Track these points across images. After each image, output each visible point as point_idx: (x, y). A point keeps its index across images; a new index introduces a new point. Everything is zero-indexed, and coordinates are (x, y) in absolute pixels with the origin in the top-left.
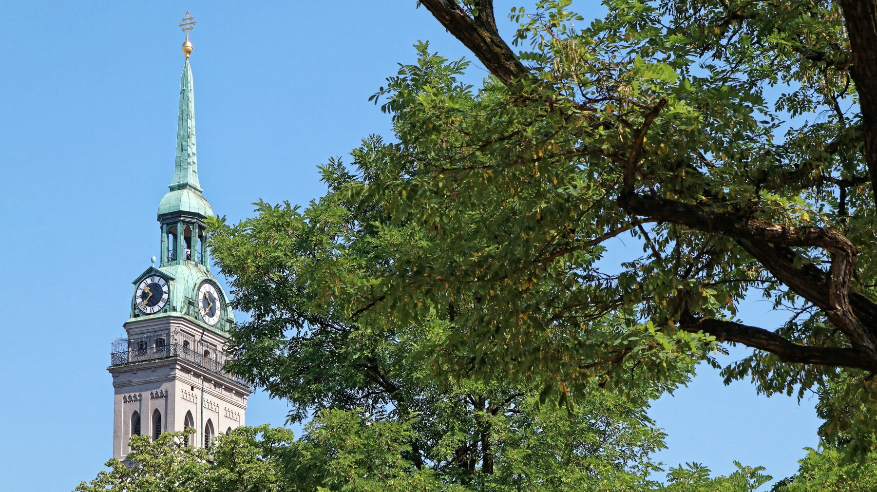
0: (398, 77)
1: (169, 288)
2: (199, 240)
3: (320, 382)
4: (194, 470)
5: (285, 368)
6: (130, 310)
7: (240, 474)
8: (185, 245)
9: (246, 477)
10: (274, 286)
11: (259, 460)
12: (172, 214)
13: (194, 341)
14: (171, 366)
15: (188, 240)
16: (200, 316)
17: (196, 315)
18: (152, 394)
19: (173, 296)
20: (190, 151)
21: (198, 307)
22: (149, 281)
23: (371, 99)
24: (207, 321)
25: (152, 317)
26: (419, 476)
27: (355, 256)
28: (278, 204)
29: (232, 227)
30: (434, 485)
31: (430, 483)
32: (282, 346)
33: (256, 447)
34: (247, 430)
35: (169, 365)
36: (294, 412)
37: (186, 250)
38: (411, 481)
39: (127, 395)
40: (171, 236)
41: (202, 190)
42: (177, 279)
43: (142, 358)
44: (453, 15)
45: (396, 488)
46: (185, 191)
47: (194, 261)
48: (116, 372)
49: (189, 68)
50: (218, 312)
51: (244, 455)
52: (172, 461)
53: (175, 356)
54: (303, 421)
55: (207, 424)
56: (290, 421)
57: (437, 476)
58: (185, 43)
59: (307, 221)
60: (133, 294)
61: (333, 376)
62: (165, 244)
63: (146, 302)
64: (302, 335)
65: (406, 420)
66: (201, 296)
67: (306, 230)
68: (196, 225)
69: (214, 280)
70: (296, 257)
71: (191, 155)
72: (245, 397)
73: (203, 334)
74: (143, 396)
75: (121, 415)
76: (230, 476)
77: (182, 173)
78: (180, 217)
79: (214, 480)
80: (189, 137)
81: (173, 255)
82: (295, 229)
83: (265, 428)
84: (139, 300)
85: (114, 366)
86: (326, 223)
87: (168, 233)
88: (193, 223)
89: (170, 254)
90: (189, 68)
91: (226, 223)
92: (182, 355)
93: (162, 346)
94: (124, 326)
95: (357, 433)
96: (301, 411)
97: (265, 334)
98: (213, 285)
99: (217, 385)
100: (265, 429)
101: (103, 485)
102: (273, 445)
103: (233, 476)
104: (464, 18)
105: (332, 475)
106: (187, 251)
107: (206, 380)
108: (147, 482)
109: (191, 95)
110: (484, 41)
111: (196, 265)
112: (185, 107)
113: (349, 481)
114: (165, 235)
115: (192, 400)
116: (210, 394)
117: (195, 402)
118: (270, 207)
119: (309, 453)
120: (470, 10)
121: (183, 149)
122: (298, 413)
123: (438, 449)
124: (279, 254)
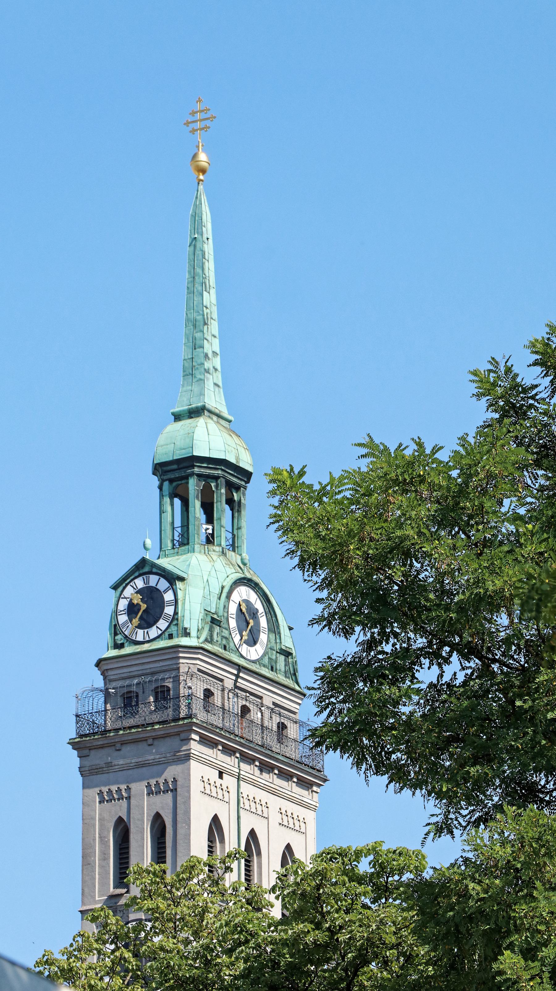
2: (227, 508)
6: (107, 636)
7: (332, 932)
8: (203, 518)
11: (365, 906)
13: (223, 690)
14: (183, 736)
16: (232, 645)
17: (224, 642)
18: (149, 786)
21: (228, 629)
22: (140, 583)
24: (244, 654)
25: (146, 647)
27: (545, 535)
28: (400, 445)
29: (317, 487)
33: (360, 884)
34: (342, 853)
35: (178, 734)
36: (440, 819)
37: (205, 526)
39: (105, 789)
40: (177, 501)
41: (230, 418)
43: (131, 722)
46: (201, 421)
47: (220, 545)
48: (85, 748)
49: (204, 199)
50: (263, 637)
51: (337, 898)
52: (205, 910)
53: (190, 716)
55: (248, 839)
56: (432, 834)
58: (195, 156)
59: (455, 473)
60: (113, 606)
63: (136, 621)
64: (447, 678)
66: (233, 609)
68: (222, 481)
69: (255, 579)
71: (210, 355)
72: (315, 788)
73: (237, 676)
74: (133, 792)
75: (94, 825)
77: (196, 388)
78: (193, 466)
79: (284, 943)
80: (205, 324)
81: (182, 535)
82: (432, 487)
83: (374, 849)
84: (123, 619)
85: (81, 736)
87: (173, 495)
88: (216, 478)
89: (176, 534)
90: (204, 199)
91: (306, 479)
92: (201, 716)
93: (165, 699)
94: (98, 665)
96: (452, 816)
98: (253, 588)
99: (265, 768)
100: (374, 850)
101: (84, 956)
102: (390, 879)
103: (321, 937)
107: (246, 759)
109: (209, 248)
111: (223, 553)
112: (199, 270)
114: (167, 500)
116: (254, 784)
117: (226, 799)
118: (386, 449)
121: (196, 345)
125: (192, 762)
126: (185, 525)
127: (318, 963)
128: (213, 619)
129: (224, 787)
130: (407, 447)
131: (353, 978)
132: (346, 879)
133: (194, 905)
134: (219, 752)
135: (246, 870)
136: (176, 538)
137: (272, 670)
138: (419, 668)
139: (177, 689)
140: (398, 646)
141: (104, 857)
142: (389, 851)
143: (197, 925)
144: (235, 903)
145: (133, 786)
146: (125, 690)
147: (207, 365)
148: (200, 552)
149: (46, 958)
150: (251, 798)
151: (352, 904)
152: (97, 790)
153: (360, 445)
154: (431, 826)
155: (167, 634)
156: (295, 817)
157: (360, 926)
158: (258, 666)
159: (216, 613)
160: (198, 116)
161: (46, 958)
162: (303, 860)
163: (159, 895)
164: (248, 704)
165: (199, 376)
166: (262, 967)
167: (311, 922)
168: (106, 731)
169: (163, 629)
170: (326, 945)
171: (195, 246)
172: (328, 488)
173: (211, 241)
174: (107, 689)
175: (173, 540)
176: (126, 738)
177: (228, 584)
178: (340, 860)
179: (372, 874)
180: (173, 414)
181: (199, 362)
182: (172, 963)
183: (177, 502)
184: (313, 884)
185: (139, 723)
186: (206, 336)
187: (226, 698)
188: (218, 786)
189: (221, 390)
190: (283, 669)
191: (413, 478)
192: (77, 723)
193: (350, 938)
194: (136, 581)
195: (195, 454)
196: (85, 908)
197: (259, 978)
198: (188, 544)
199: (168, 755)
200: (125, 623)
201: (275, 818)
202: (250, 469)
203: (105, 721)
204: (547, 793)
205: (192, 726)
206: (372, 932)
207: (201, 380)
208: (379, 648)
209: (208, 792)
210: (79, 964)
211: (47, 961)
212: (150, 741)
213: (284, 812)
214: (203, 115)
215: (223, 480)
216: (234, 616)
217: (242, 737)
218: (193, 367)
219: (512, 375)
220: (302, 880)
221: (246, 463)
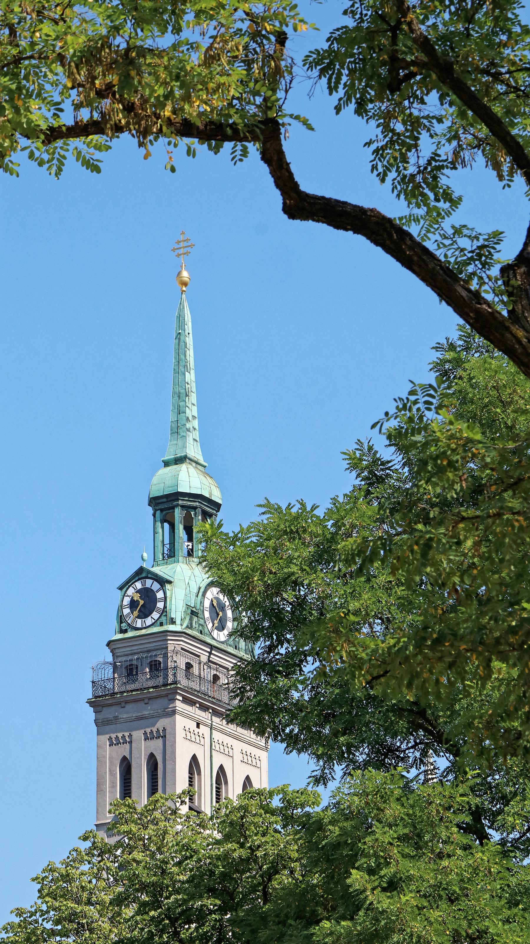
0: (407, 399)
1: (165, 593)
3: (351, 733)
4: (193, 846)
5: (305, 715)
6: (115, 624)
8: (185, 537)
9: (260, 853)
10: (289, 609)
11: (276, 831)
12: (167, 496)
13: (200, 663)
14: (170, 697)
15: (189, 530)
16: (206, 630)
17: (201, 628)
18: (145, 733)
19: (171, 604)
20: (189, 414)
21: (204, 618)
22: (139, 585)
23: (373, 427)
25: (143, 632)
26: (480, 854)
28: (290, 504)
29: (231, 535)
30: (502, 866)
31: (496, 863)
32: (300, 687)
35: (167, 695)
36: (318, 773)
37: (186, 544)
38: (471, 862)
39: (113, 736)
40: (166, 525)
42: (176, 582)
43: (132, 687)
44: (479, 313)
45: (451, 870)
46: (184, 467)
48: (99, 706)
49: (186, 304)
51: (256, 825)
52: (165, 832)
53: (175, 683)
54: (330, 784)
56: (312, 784)
57: (505, 854)
58: (179, 273)
60: (119, 602)
61: (367, 725)
62: (159, 536)
63: (136, 613)
65: (462, 782)
66: (207, 604)
67: (329, 536)
68: (199, 511)
70: (315, 572)
71: (190, 418)
73: (210, 653)
74: (134, 737)
75: (106, 762)
76: (239, 853)
77: (180, 442)
78: (178, 500)
79: (218, 858)
80: (187, 395)
83: (283, 790)
84: (126, 611)
85: (96, 697)
86: (353, 526)
87: (163, 521)
88: (195, 508)
89: (166, 549)
90: (186, 304)
92: (183, 682)
93: (157, 670)
94: (108, 645)
95: (398, 799)
96: (326, 771)
97: (279, 672)
100: (283, 791)
101: (77, 865)
102: (295, 811)
103: (244, 853)
104: (495, 314)
105: (368, 856)
106: (187, 545)
107: (216, 713)
108: (134, 860)
109: (190, 341)
110: (520, 342)
112: (182, 357)
113: (390, 863)
114: (159, 524)
115: (198, 741)
116: (222, 732)
117: (202, 743)
118: (280, 508)
119: (337, 828)
120: (502, 301)
121: (180, 411)
122: (324, 773)
123: (504, 819)
124: (294, 569)
125: (177, 716)
126: (172, 542)
127: (243, 872)
128: (192, 611)
129: (201, 735)
130: (294, 506)
131: (268, 883)
132: (263, 812)
133: (158, 829)
134: (197, 709)
135: (216, 795)
136: (166, 552)
137: (236, 648)
138: (305, 664)
139: (166, 662)
140: (290, 650)
141: (113, 786)
142: (294, 791)
143: (160, 843)
144: (188, 827)
145: (134, 733)
146: (128, 663)
147: (188, 425)
148: (183, 562)
149: (50, 867)
150: (220, 742)
151: (267, 829)
152: (108, 736)
153: (260, 506)
154: (311, 779)
155: (158, 622)
156: (253, 756)
157: (273, 846)
158: (225, 646)
159: (195, 607)
160: (181, 245)
161: (50, 867)
162: (232, 798)
163: (133, 822)
164: (218, 674)
165: (182, 434)
166: (202, 876)
167: (238, 843)
168: (114, 693)
169: (156, 619)
170: (248, 860)
171: (179, 339)
172: (240, 535)
173: (191, 335)
174: (115, 663)
175: (163, 554)
176: (129, 699)
177: (203, 585)
178: (258, 797)
179: (282, 808)
180: (163, 461)
181: (182, 423)
182: (137, 873)
183: (166, 526)
184: (239, 815)
185: (138, 688)
186: (187, 404)
187: (202, 669)
188: (196, 733)
189: (199, 444)
190: (244, 648)
191: (297, 529)
192: (93, 687)
193: (265, 854)
194: (136, 583)
195: (180, 490)
196: (99, 823)
197: (200, 883)
198: (174, 556)
199: (159, 711)
200: (128, 614)
201: (238, 757)
202: (220, 501)
203: (114, 686)
204: (402, 751)
205: (177, 690)
206: (281, 850)
207: (183, 436)
208: (276, 651)
209: (189, 737)
210: (74, 871)
211: (51, 869)
212: (146, 701)
213: (244, 753)
214: (186, 244)
215: (200, 510)
216: (208, 609)
217: (214, 698)
218: (178, 427)
219: (373, 452)
220: (230, 812)
221: (217, 496)
